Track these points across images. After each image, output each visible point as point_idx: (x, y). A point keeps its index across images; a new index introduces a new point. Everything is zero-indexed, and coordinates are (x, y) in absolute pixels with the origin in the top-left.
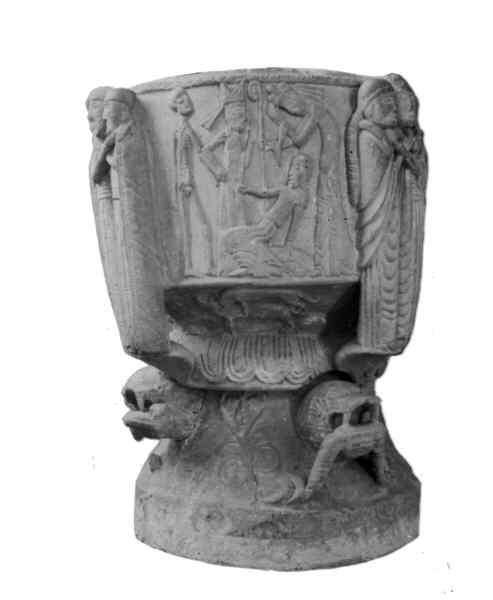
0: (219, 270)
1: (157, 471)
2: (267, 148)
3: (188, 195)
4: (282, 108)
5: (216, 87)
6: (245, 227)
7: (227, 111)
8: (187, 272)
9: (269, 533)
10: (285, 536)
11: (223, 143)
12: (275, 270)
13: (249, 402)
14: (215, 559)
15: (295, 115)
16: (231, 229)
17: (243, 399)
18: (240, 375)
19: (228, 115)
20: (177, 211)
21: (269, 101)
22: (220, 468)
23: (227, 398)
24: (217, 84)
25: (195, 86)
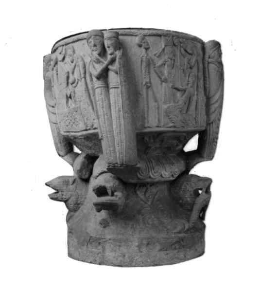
0: (163, 124)
1: (107, 228)
2: (182, 68)
3: (148, 88)
4: (186, 51)
5: (159, 37)
6: (173, 104)
7: (165, 49)
8: (146, 125)
9: (177, 247)
10: (183, 247)
11: (165, 64)
12: (183, 125)
13: (151, 188)
14: (152, 264)
15: (190, 54)
16: (168, 105)
17: (148, 186)
18: (155, 175)
19: (166, 51)
20: (142, 95)
21: (181, 46)
22: (143, 221)
23: (140, 187)
24: (160, 36)
25: (149, 35)
